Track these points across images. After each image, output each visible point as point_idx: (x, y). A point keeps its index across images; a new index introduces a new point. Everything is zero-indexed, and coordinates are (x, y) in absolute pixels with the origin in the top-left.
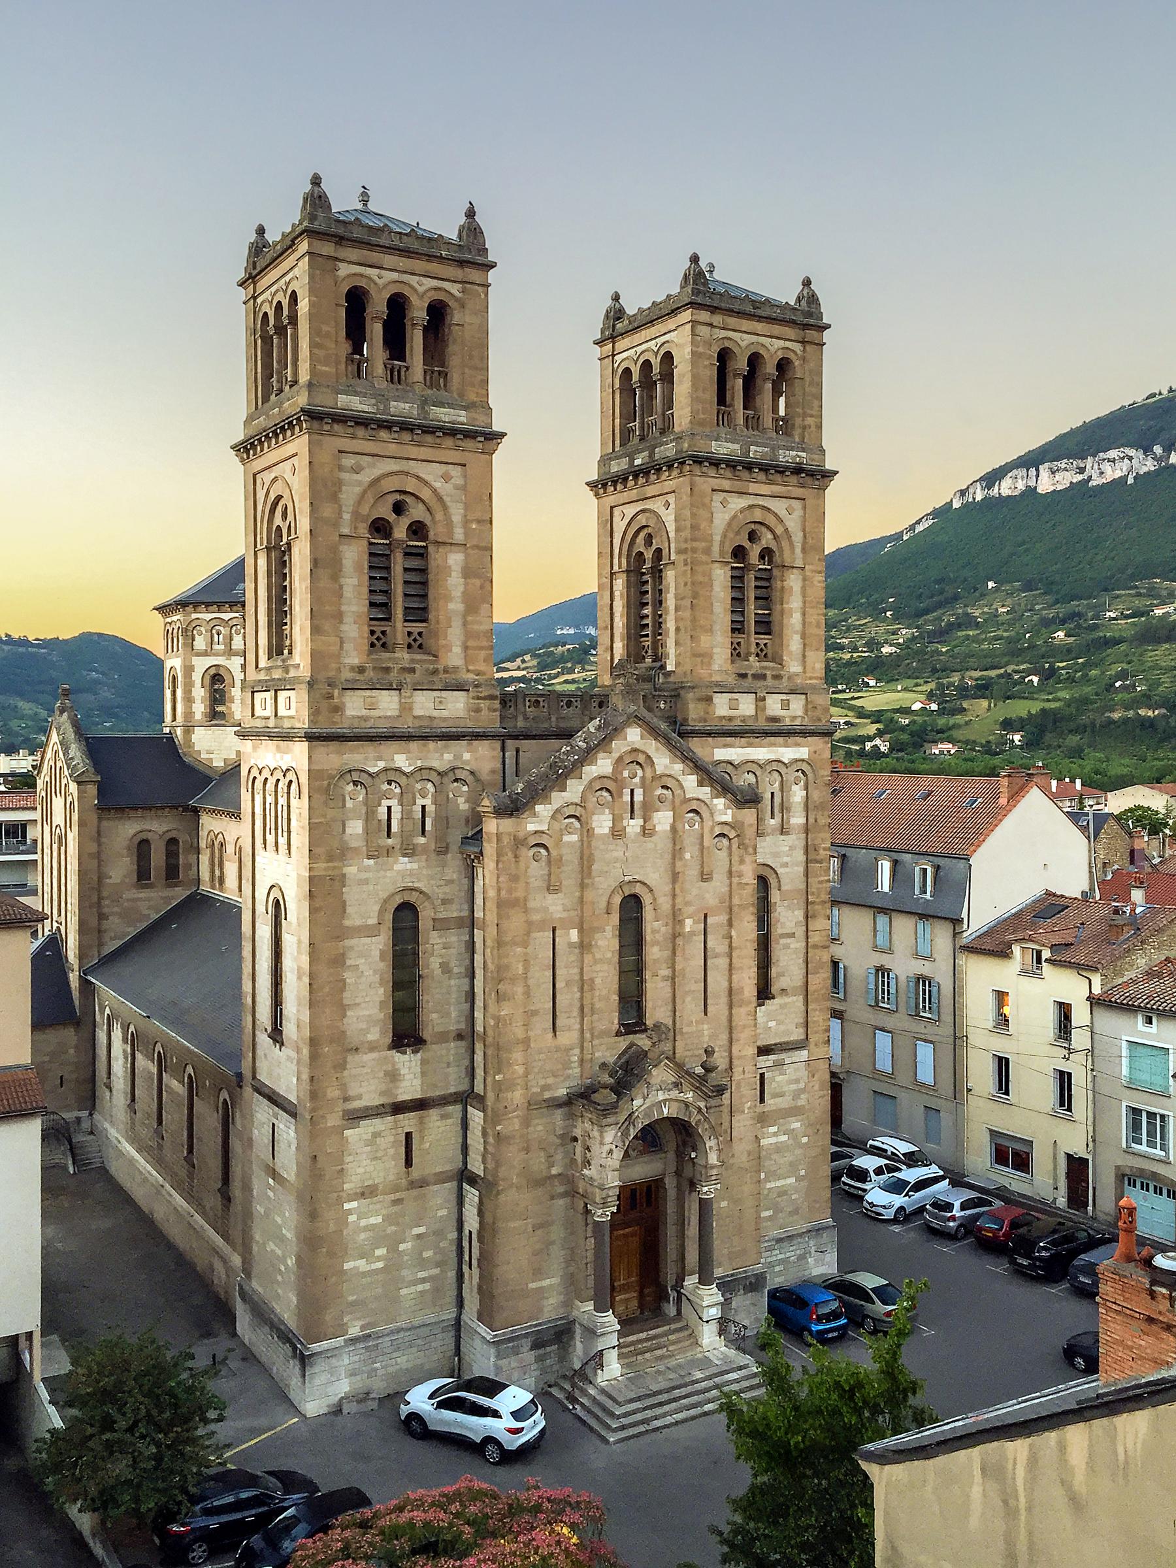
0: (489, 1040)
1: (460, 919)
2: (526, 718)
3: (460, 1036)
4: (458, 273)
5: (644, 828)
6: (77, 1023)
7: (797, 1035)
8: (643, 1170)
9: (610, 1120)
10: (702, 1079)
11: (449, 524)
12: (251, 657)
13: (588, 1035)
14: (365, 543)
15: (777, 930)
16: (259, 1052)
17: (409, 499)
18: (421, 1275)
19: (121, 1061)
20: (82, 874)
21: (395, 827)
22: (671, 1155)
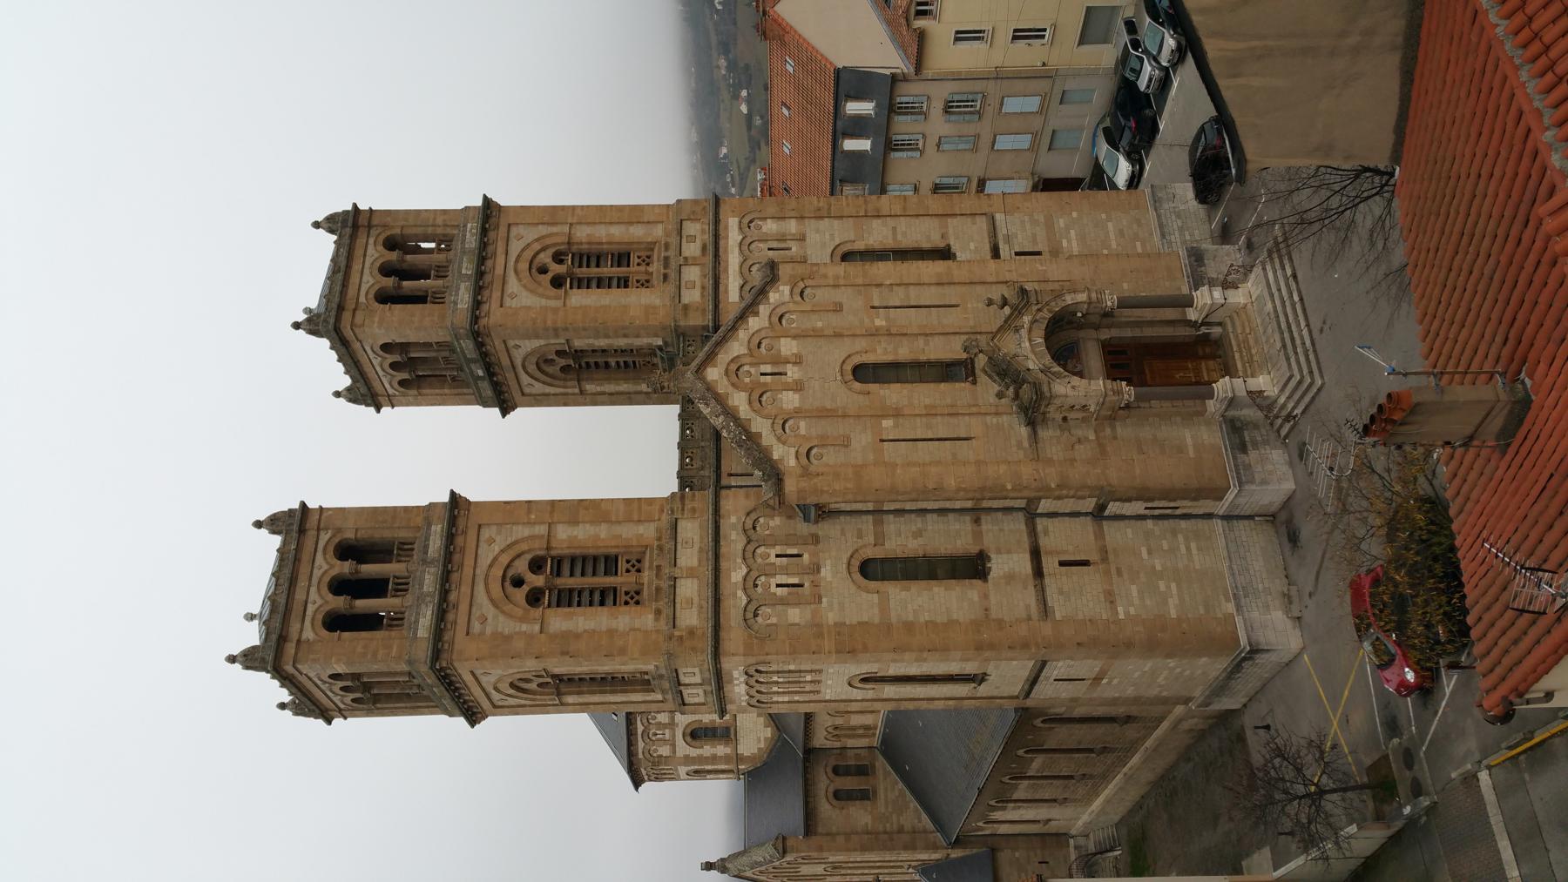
0: (978, 495)
1: (875, 523)
2: (702, 468)
3: (977, 521)
4: (311, 534)
5: (795, 363)
6: (993, 850)
7: (982, 223)
8: (1093, 358)
9: (1045, 389)
10: (1014, 309)
11: (532, 537)
12: (654, 707)
13: (974, 410)
14: (548, 611)
15: (890, 243)
16: (995, 693)
17: (510, 573)
18: (1183, 548)
19: (1022, 812)
20: (864, 849)
21: (795, 580)
22: (1082, 334)
